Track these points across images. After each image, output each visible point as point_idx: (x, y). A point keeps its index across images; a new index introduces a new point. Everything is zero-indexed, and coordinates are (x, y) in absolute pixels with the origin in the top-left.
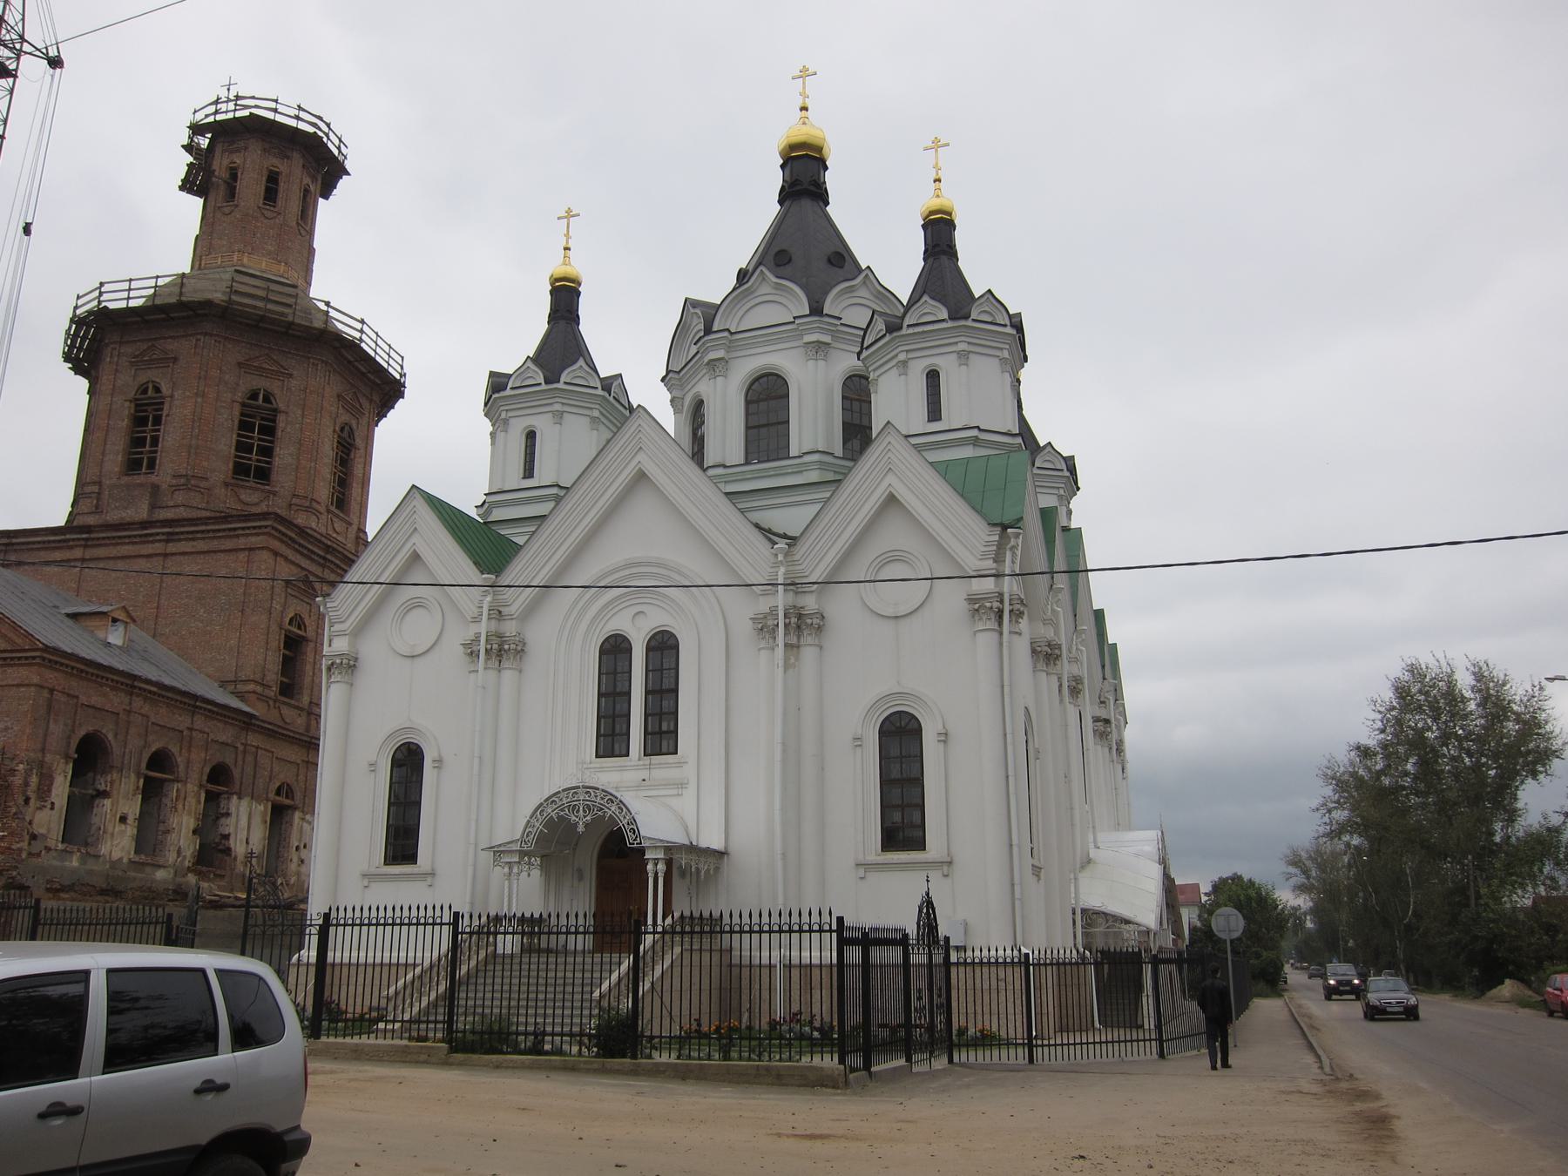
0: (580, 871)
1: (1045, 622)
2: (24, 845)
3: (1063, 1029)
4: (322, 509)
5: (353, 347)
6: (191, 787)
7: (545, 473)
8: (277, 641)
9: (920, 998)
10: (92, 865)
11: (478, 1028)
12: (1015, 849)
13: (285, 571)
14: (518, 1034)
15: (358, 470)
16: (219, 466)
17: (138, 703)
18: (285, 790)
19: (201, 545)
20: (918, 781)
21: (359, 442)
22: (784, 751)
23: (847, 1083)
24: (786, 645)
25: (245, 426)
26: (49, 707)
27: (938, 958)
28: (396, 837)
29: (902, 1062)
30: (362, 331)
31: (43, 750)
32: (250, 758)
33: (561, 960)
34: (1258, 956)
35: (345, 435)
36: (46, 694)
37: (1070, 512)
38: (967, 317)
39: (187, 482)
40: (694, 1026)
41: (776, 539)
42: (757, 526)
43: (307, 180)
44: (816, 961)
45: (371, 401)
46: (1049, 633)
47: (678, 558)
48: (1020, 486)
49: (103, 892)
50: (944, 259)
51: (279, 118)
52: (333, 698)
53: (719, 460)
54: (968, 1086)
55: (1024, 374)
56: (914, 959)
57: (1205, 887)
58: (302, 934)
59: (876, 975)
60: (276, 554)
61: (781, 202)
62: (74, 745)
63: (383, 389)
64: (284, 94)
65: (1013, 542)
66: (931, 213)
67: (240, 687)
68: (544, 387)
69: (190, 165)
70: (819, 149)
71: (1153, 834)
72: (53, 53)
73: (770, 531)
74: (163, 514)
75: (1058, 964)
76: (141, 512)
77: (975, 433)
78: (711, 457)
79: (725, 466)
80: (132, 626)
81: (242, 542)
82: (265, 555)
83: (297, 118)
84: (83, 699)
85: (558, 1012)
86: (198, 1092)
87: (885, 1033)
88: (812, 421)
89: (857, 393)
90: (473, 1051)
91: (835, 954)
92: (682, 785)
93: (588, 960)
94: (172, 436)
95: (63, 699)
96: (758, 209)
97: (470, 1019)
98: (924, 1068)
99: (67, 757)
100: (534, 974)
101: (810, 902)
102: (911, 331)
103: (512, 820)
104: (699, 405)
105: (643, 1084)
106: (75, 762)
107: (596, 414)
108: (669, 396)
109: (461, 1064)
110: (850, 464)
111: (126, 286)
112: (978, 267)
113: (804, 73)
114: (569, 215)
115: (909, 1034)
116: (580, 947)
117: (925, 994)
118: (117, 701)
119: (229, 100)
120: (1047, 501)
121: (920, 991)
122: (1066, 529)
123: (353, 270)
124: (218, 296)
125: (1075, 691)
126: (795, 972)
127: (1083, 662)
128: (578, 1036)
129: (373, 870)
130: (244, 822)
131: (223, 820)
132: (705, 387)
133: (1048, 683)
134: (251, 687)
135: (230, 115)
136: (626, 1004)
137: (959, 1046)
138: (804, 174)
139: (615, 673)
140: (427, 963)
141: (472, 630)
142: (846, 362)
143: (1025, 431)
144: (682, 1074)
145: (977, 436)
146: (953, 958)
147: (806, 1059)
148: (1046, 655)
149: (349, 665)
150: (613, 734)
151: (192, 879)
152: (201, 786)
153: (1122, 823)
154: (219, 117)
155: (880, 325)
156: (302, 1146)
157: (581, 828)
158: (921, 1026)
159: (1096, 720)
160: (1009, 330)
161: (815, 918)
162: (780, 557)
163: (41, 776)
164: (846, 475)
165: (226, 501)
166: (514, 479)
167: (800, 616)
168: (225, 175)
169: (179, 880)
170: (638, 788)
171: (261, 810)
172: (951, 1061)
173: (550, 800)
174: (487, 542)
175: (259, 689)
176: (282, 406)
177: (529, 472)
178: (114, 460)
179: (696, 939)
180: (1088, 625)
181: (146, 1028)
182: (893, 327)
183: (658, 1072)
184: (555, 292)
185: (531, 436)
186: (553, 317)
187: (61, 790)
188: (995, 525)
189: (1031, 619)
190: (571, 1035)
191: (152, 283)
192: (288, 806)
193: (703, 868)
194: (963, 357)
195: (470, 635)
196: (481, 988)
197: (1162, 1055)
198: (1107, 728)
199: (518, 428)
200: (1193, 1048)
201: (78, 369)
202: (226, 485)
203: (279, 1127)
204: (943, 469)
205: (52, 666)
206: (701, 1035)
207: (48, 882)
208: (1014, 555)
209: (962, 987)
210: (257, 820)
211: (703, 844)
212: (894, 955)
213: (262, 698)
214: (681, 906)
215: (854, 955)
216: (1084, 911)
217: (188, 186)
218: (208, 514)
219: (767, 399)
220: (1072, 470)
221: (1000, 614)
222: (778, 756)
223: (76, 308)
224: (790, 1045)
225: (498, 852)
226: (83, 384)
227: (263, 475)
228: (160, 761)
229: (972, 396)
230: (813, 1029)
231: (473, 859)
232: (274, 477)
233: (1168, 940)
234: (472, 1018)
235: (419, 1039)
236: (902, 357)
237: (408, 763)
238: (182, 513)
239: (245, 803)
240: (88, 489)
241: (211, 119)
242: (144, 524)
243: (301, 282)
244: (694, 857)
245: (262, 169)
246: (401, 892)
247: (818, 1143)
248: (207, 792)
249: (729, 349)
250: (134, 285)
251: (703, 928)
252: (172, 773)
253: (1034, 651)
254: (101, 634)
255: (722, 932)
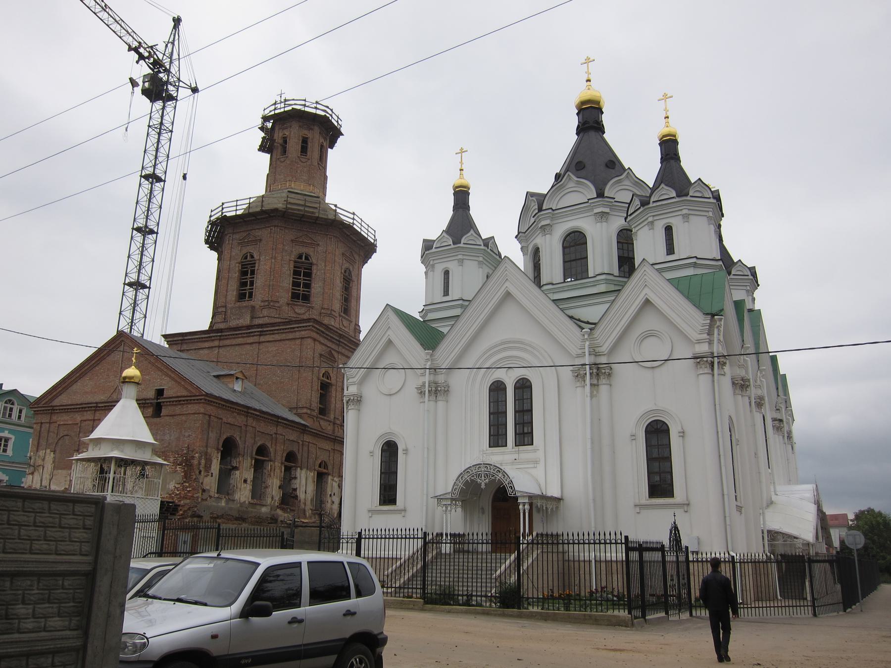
0: (483, 509)
1: (739, 367)
2: (200, 495)
3: (758, 599)
4: (337, 315)
5: (349, 228)
6: (277, 464)
7: (455, 292)
8: (317, 386)
9: (672, 580)
10: (231, 505)
11: (438, 592)
12: (726, 497)
13: (319, 348)
14: (458, 595)
15: (354, 293)
16: (285, 296)
17: (250, 421)
18: (324, 465)
19: (277, 337)
20: (668, 459)
21: (354, 278)
22: (592, 443)
23: (633, 625)
24: (591, 385)
25: (296, 273)
26: (209, 424)
27: (682, 558)
28: (385, 490)
29: (663, 614)
30: (353, 219)
31: (207, 446)
32: (305, 448)
33: (475, 557)
34: (884, 558)
35: (347, 274)
36: (207, 417)
37: (754, 299)
38: (687, 195)
39: (269, 304)
40: (550, 593)
41: (583, 325)
42: (571, 317)
43: (322, 140)
44: (614, 559)
45: (359, 255)
46: (742, 373)
47: (530, 338)
48: (722, 290)
49: (237, 519)
50: (672, 162)
51: (307, 109)
52: (350, 417)
53: (549, 281)
54: (700, 628)
55: (723, 223)
56: (668, 559)
57: (851, 516)
58: (339, 543)
59: (647, 570)
60: (315, 340)
61: (578, 134)
62: (221, 444)
63: (361, 247)
64: (308, 94)
65: (718, 323)
66: (664, 136)
67: (300, 411)
68: (453, 246)
69: (263, 138)
70: (598, 103)
71: (811, 487)
72: (193, 85)
73: (579, 320)
74: (257, 322)
75: (755, 562)
76: (246, 320)
77: (694, 260)
78: (544, 280)
79: (553, 284)
80: (245, 381)
81: (297, 335)
82: (309, 341)
83: (316, 108)
84: (225, 419)
85: (475, 584)
86: (290, 623)
87: (654, 599)
88: (601, 256)
89: (625, 240)
90: (436, 604)
91: (624, 555)
92: (536, 462)
93: (489, 557)
94: (260, 281)
95: (215, 420)
96: (565, 138)
97: (434, 587)
98: (676, 618)
99: (218, 449)
100: (461, 564)
101: (610, 528)
102: (655, 204)
103: (446, 481)
104: (537, 251)
105: (525, 622)
106: (222, 452)
107: (481, 259)
108: (519, 246)
109: (430, 610)
110: (625, 280)
111: (235, 204)
112: (693, 165)
113: (588, 61)
114: (462, 151)
115: (667, 600)
116: (484, 550)
117: (675, 578)
118: (240, 420)
119: (281, 102)
120: (738, 295)
121: (672, 576)
122: (751, 311)
123: (348, 187)
124: (280, 206)
125: (760, 404)
126: (603, 565)
127: (763, 387)
128: (490, 598)
129: (374, 508)
130: (304, 482)
131: (293, 481)
132: (539, 240)
133: (742, 401)
134: (305, 411)
135: (282, 110)
136: (513, 579)
137: (696, 607)
138: (590, 117)
139: (498, 401)
140: (407, 556)
141: (422, 380)
142: (618, 222)
143: (725, 254)
144: (545, 618)
145: (696, 262)
146: (691, 559)
147: (610, 612)
148: (741, 385)
149: (358, 400)
150: (498, 435)
151: (279, 512)
152: (282, 463)
153: (792, 479)
154: (277, 112)
155: (637, 202)
156: (384, 641)
157: (483, 486)
158: (673, 596)
159: (774, 420)
160: (712, 200)
161: (613, 536)
162: (586, 337)
163: (206, 459)
164: (623, 286)
165: (288, 313)
166: (439, 297)
167: (598, 369)
168: (281, 141)
169: (273, 512)
170: (512, 464)
171: (312, 475)
172: (691, 615)
173: (466, 471)
174: (426, 332)
175: (309, 412)
176: (314, 261)
177: (446, 293)
178: (232, 294)
179: (550, 546)
180: (767, 365)
181: (287, 590)
182: (645, 203)
183: (531, 616)
184: (456, 194)
185: (447, 273)
186: (456, 208)
187: (215, 467)
188: (707, 314)
189: (731, 366)
190: (486, 596)
191: (248, 201)
192: (328, 471)
193: (550, 507)
194: (686, 217)
195: (420, 383)
196: (434, 571)
197: (815, 615)
198: (782, 424)
199: (440, 268)
200: (834, 611)
201: (212, 248)
202: (288, 304)
203: (376, 632)
204: (676, 283)
205: (209, 403)
206: (553, 598)
207: (212, 513)
208: (719, 331)
209: (696, 573)
210: (310, 480)
211: (549, 494)
212: (657, 556)
213: (310, 416)
214: (538, 529)
215: (634, 556)
216: (769, 532)
217: (262, 148)
218: (280, 320)
219: (575, 244)
220: (754, 275)
221: (712, 364)
222: (589, 446)
223: (211, 216)
224: (601, 604)
225: (439, 499)
226: (215, 255)
227: (306, 298)
228: (262, 450)
229: (693, 240)
230: (614, 596)
231: (426, 504)
232: (312, 299)
233: (823, 549)
234: (433, 584)
235: (408, 597)
236: (650, 219)
237: (390, 451)
238: (266, 320)
239: (304, 471)
240: (220, 310)
241: (273, 113)
242: (248, 327)
243: (321, 194)
244: (544, 501)
245: (299, 136)
246: (388, 521)
247: (618, 653)
248: (285, 467)
249: (552, 219)
250: (239, 203)
251: (552, 541)
252: (267, 456)
253: (733, 383)
254: (231, 386)
255: (563, 543)
